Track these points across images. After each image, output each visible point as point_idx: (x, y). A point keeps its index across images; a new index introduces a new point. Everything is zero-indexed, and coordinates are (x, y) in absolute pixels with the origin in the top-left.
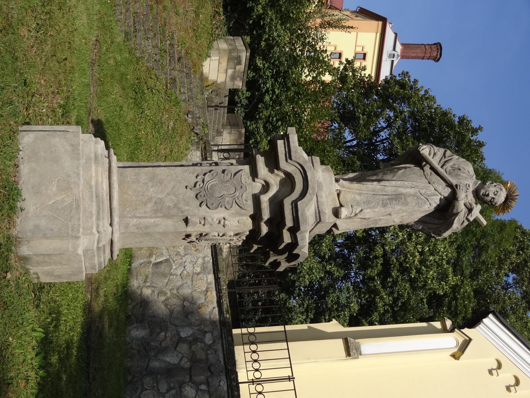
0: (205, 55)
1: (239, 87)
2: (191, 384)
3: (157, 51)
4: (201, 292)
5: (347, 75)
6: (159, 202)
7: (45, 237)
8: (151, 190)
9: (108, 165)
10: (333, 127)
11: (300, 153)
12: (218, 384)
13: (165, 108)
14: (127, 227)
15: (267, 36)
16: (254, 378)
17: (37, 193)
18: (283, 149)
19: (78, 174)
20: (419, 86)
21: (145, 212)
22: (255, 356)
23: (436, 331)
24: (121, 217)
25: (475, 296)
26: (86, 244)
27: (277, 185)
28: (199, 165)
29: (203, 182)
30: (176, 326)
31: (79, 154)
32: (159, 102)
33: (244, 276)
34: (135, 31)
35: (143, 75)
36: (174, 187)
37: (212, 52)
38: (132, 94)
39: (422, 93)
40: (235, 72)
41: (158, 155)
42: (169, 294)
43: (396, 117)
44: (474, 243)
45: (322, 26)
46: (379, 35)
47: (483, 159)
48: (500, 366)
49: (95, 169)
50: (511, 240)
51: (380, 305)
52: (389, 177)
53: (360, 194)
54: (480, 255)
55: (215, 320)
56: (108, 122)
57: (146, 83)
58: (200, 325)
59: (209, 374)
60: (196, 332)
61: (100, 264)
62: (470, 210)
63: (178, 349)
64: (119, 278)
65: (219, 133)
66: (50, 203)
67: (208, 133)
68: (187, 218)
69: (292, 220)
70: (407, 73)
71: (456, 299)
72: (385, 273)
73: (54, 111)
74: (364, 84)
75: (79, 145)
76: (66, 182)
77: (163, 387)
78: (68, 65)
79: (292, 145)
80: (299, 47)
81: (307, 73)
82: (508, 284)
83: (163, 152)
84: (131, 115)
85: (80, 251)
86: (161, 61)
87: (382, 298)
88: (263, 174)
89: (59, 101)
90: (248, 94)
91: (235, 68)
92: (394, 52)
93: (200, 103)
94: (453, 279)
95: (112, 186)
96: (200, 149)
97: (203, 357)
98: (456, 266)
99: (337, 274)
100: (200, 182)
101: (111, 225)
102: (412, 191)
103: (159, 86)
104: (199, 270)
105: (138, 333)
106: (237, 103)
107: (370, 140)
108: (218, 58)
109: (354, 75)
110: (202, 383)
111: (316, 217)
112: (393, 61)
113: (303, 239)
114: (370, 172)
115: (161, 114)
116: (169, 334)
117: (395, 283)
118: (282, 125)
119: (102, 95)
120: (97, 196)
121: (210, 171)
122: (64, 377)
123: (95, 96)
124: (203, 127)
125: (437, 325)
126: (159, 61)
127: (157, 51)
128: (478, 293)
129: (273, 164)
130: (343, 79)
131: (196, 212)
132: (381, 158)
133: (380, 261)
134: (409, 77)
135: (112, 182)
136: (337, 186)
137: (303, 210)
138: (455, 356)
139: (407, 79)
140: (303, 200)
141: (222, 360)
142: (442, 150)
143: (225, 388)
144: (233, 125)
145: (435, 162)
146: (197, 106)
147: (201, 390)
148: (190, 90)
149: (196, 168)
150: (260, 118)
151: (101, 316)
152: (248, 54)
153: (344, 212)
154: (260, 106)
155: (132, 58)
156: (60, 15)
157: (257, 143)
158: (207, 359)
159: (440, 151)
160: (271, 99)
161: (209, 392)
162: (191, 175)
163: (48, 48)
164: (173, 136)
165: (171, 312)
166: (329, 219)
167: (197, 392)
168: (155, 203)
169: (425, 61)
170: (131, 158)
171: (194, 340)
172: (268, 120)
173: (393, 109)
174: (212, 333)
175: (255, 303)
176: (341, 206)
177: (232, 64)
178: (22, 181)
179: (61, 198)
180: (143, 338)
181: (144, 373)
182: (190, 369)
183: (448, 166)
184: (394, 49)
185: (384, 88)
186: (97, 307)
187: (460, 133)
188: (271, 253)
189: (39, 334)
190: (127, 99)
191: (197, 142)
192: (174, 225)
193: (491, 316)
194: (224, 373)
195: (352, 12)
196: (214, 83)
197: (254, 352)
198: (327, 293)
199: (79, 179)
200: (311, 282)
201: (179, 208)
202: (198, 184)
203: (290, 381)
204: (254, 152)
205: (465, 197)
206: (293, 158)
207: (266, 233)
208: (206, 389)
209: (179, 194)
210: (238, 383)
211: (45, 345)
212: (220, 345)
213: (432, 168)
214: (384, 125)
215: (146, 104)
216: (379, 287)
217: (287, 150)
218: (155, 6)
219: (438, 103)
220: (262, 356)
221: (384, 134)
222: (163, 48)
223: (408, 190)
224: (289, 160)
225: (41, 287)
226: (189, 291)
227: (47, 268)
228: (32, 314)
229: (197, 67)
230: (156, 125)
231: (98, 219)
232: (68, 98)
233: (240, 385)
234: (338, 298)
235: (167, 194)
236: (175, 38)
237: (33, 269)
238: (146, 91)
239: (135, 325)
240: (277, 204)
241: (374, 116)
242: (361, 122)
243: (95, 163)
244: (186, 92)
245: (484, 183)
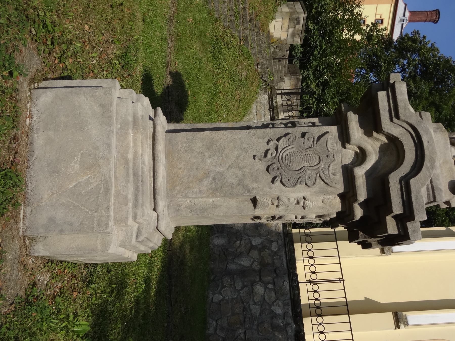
0: (271, 18)
1: (298, 42)
2: (260, 283)
3: (232, 13)
5: (372, 35)
6: (218, 178)
8: (209, 161)
9: (152, 130)
10: (361, 73)
12: (282, 284)
13: (239, 60)
14: (178, 210)
15: (317, 5)
16: (311, 279)
17: (54, 172)
18: (386, 104)
19: (109, 146)
20: (427, 40)
21: (200, 192)
26: (121, 238)
27: (376, 153)
28: (271, 126)
29: (277, 149)
30: (249, 236)
31: (110, 117)
32: (234, 56)
35: (220, 33)
36: (238, 157)
37: (277, 15)
38: (210, 49)
39: (429, 46)
40: (294, 31)
41: (234, 99)
43: (409, 64)
46: (393, 5)
49: (134, 136)
55: (279, 231)
56: (187, 73)
57: (223, 40)
58: (268, 235)
59: (275, 275)
60: (265, 241)
63: (250, 254)
65: (282, 80)
66: (71, 186)
67: (273, 80)
68: (255, 198)
69: (401, 205)
70: (418, 31)
74: (384, 41)
75: (111, 105)
76: (93, 156)
77: (239, 285)
78: (125, 10)
79: (399, 97)
80: (341, 12)
81: (347, 32)
83: (238, 96)
84: (210, 66)
86: (236, 22)
88: (356, 138)
89: (115, 51)
91: (295, 28)
92: (404, 18)
95: (156, 158)
96: (267, 93)
97: (270, 262)
100: (273, 151)
103: (234, 42)
106: (294, 56)
108: (281, 19)
109: (377, 34)
110: (269, 283)
111: (428, 195)
112: (403, 24)
115: (235, 66)
116: (243, 243)
118: (327, 72)
119: (179, 50)
121: (286, 135)
123: (172, 49)
124: (270, 75)
126: (234, 21)
127: (232, 13)
129: (371, 124)
130: (369, 37)
134: (419, 34)
135: (156, 152)
139: (417, 36)
140: (417, 177)
141: (285, 264)
143: (288, 288)
144: (292, 73)
146: (265, 58)
147: (269, 288)
148: (260, 45)
149: (268, 130)
150: (310, 67)
152: (306, 15)
154: (311, 58)
155: (211, 19)
158: (273, 263)
160: (319, 53)
161: (275, 290)
162: (261, 140)
164: (246, 84)
167: (265, 290)
168: (214, 179)
169: (427, 23)
170: (211, 103)
171: (263, 248)
172: (316, 68)
174: (277, 242)
177: (292, 24)
178: (35, 157)
179: (85, 179)
180: (223, 245)
181: (224, 273)
182: (260, 271)
184: (404, 16)
188: (361, 233)
190: (207, 53)
191: (265, 88)
194: (287, 275)
196: (278, 40)
199: (110, 152)
201: (245, 186)
202: (270, 152)
203: (340, 282)
204: (343, 108)
206: (401, 116)
207: (361, 217)
208: (273, 288)
209: (244, 167)
210: (298, 283)
212: (283, 252)
215: (223, 57)
217: (392, 105)
219: (441, 53)
220: (319, 268)
222: (237, 10)
224: (395, 120)
229: (264, 27)
230: (231, 74)
231: (136, 206)
233: (300, 284)
235: (229, 166)
236: (247, 3)
238: (223, 46)
239: (216, 235)
241: (393, 64)
242: (383, 68)
243: (134, 128)
244: (256, 47)
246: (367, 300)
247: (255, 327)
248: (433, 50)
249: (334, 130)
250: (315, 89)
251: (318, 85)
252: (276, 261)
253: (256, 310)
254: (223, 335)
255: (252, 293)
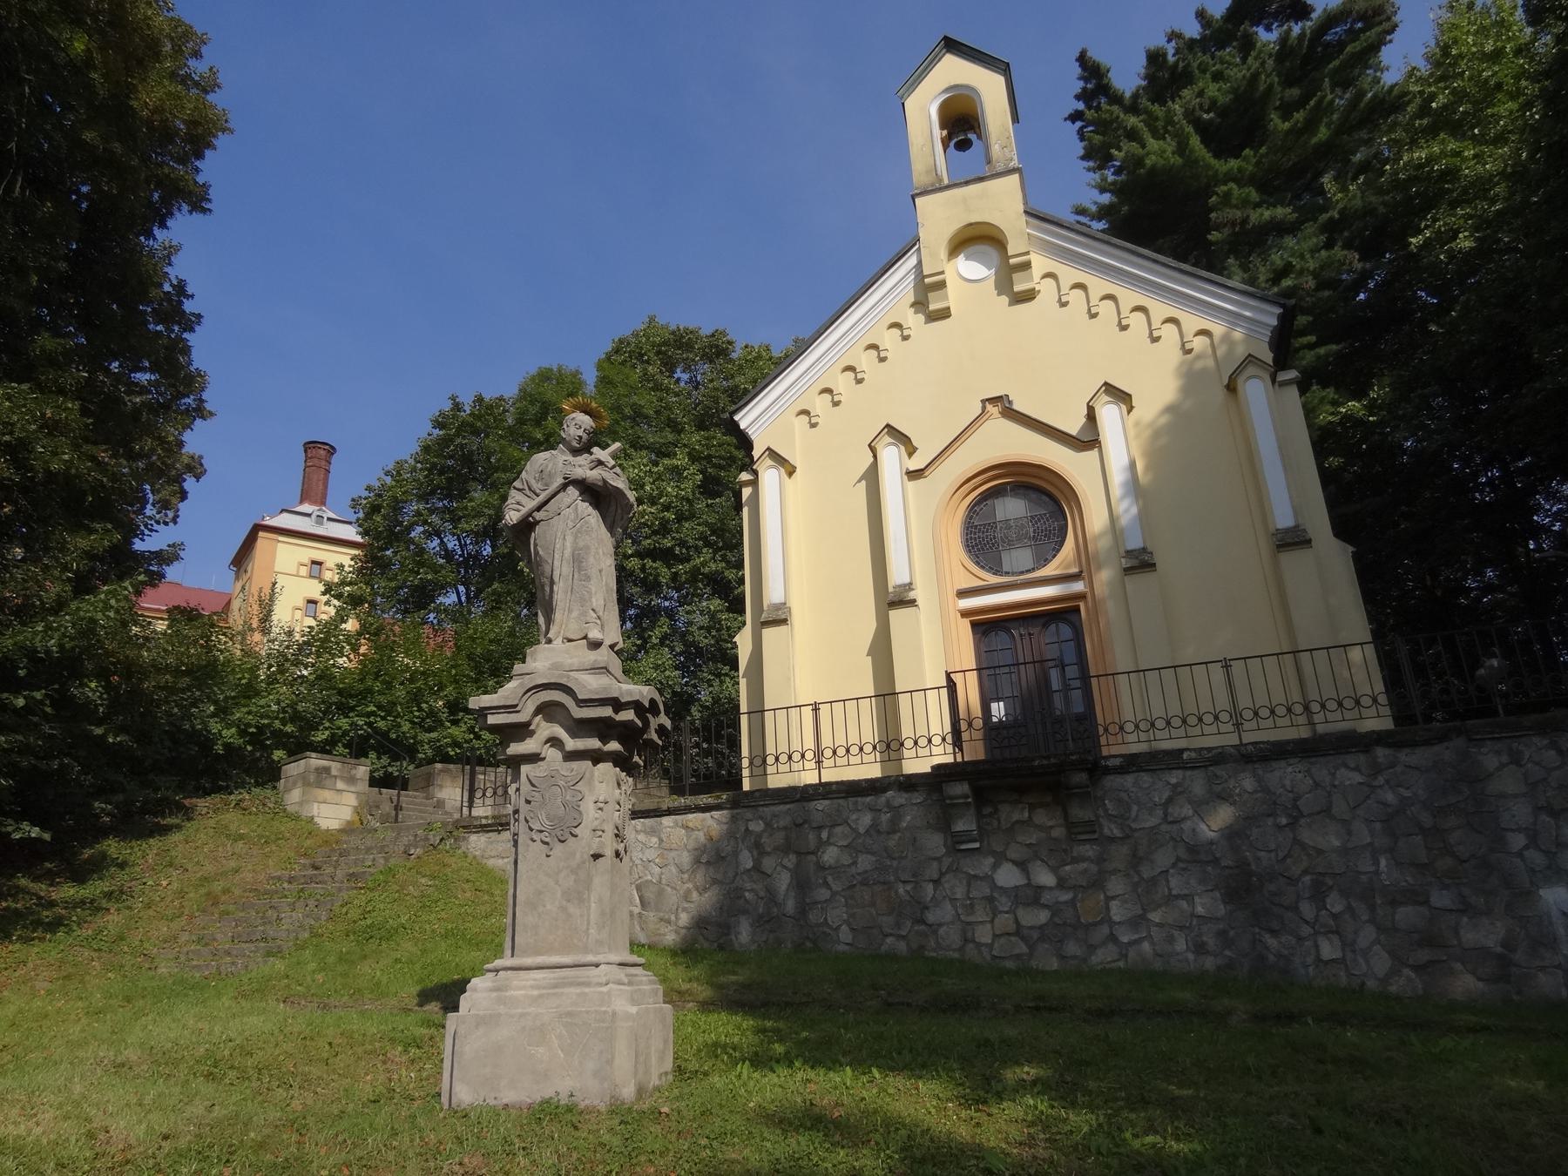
4: (689, 837)
7: (610, 1062)
11: (510, 691)
19: (522, 1015)
22: (783, 758)
23: (755, 496)
24: (586, 950)
25: (707, 429)
33: (666, 772)
34: (265, 940)
37: (305, 813)
39: (388, 480)
40: (342, 778)
42: (690, 885)
43: (425, 522)
44: (628, 424)
45: (265, 631)
47: (501, 399)
48: (805, 412)
50: (626, 370)
51: (713, 566)
52: (547, 569)
53: (570, 611)
54: (646, 417)
56: (421, 980)
61: (651, 982)
62: (600, 463)
64: (663, 960)
65: (440, 804)
71: (709, 457)
72: (666, 556)
73: (413, 1061)
77: (823, 894)
82: (690, 381)
83: (468, 895)
85: (634, 1010)
87: (704, 564)
90: (373, 755)
93: (391, 835)
94: (681, 459)
97: (782, 834)
98: (662, 452)
99: (665, 629)
100: (542, 836)
101: (597, 966)
102: (569, 539)
104: (655, 840)
105: (744, 933)
107: (459, 564)
109: (350, 584)
113: (630, 692)
114: (539, 595)
116: (748, 886)
117: (682, 543)
120: (555, 986)
122: (805, 1034)
125: (746, 492)
127: (301, 903)
128: (701, 426)
129: (522, 731)
130: (355, 601)
131: (586, 841)
132: (489, 549)
133: (649, 563)
136: (558, 642)
137: (591, 691)
138: (791, 471)
142: (513, 492)
144: (428, 783)
145: (530, 504)
148: (368, 850)
150: (414, 738)
151: (720, 987)
152: (314, 755)
153: (595, 634)
156: (261, 1054)
157: (455, 744)
158: (785, 828)
159: (514, 496)
160: (383, 718)
163: (315, 1071)
165: (715, 882)
166: (603, 656)
171: (758, 849)
173: (410, 528)
175: (707, 753)
176: (585, 637)
177: (328, 782)
182: (798, 853)
183: (536, 486)
184: (309, 515)
185: (377, 537)
186: (705, 992)
187: (459, 429)
189: (745, 1069)
192: (601, 876)
193: (736, 418)
195: (237, 578)
196: (357, 811)
197: (777, 759)
198: (694, 644)
200: (677, 668)
205: (582, 467)
210: (821, 784)
211: (760, 1061)
213: (539, 509)
214: (436, 542)
216: (688, 566)
218: (222, 907)
221: (452, 543)
223: (568, 544)
225: (679, 1070)
226: (685, 853)
227: (654, 1060)
228: (716, 1080)
230: (424, 906)
231: (588, 984)
232: (392, 1040)
234: (701, 628)
237: (654, 1081)
238: (369, 922)
240: (580, 727)
245: (563, 441)
246: (872, 652)
247: (895, 863)
248: (399, 473)
249: (525, 769)
250: (464, 728)
251: (455, 723)
252: (782, 824)
253: (865, 862)
254: (909, 923)
255: (836, 870)
